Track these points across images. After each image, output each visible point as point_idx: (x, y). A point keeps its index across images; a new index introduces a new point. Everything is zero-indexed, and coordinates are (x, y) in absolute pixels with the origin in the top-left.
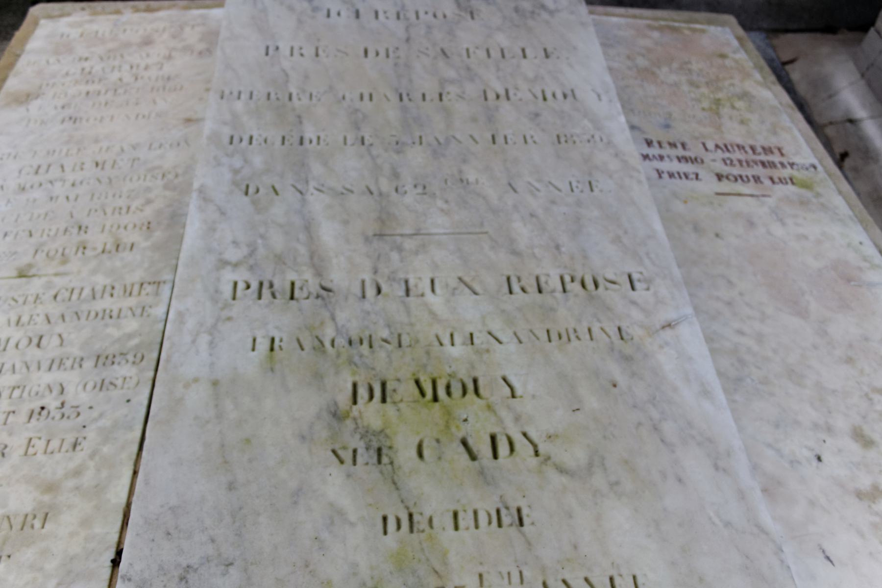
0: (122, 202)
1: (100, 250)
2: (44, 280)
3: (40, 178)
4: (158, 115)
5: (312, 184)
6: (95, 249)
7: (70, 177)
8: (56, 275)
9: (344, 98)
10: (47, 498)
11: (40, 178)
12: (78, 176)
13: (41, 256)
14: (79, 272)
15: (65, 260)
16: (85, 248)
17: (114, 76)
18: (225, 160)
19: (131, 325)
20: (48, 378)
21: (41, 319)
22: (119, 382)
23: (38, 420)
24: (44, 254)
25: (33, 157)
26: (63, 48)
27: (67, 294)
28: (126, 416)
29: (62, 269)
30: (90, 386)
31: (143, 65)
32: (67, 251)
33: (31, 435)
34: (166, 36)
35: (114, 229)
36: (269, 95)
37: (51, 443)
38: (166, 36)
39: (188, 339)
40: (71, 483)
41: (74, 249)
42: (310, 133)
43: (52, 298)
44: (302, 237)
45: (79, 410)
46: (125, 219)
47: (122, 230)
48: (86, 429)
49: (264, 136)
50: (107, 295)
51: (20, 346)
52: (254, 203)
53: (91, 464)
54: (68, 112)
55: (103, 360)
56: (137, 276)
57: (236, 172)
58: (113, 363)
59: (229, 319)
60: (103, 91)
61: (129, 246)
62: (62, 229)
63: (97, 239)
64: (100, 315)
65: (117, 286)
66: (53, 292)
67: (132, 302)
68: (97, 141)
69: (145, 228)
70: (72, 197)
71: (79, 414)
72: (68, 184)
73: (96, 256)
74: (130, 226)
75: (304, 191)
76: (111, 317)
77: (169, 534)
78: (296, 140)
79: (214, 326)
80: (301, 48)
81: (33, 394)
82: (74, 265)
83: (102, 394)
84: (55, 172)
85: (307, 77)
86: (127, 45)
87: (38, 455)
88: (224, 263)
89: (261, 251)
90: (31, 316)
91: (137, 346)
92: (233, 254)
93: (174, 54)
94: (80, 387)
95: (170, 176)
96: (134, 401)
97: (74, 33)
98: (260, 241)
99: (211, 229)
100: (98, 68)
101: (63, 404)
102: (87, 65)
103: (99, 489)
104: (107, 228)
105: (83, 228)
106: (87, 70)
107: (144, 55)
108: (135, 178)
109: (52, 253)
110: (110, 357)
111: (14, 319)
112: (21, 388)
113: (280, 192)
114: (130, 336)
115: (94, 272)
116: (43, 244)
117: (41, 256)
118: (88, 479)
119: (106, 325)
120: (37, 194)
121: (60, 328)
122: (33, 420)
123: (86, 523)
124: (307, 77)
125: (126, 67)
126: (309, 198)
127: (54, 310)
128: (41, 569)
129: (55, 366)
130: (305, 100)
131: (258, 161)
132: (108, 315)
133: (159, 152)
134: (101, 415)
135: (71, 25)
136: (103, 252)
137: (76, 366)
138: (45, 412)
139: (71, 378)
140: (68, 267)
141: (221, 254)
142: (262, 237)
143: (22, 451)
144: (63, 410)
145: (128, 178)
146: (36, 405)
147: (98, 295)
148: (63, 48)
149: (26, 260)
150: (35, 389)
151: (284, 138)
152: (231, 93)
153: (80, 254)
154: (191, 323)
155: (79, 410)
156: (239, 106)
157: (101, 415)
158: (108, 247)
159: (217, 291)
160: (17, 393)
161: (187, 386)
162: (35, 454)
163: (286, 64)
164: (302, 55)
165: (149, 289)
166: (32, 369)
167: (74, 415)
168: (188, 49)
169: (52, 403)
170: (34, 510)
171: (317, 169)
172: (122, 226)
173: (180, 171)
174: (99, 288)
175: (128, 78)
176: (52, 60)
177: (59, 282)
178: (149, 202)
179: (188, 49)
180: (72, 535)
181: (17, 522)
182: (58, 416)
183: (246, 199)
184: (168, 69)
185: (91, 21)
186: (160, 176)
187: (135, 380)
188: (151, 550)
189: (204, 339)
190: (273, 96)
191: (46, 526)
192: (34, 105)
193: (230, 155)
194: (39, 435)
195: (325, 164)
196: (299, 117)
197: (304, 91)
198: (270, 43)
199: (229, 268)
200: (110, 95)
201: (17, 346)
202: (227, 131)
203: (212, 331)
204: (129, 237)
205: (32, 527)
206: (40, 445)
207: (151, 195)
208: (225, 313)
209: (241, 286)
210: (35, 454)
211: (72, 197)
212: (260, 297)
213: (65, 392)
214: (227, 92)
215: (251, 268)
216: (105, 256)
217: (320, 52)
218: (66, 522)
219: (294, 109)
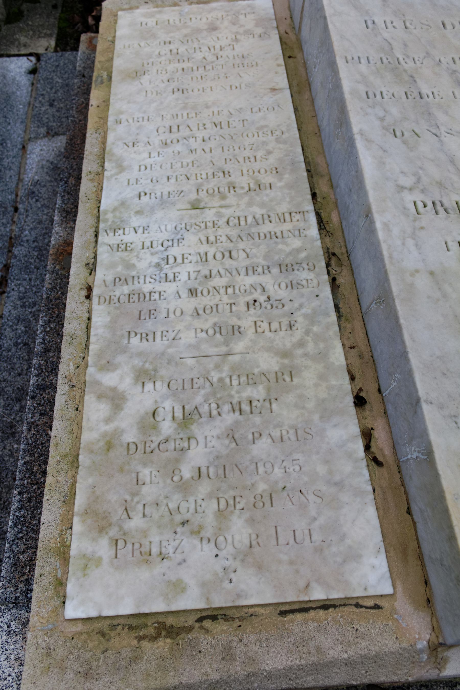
0: (247, 153)
1: (247, 189)
2: (213, 211)
3: (174, 136)
4: (247, 86)
5: (443, 129)
6: (243, 188)
7: (200, 135)
8: (221, 207)
9: (440, 61)
10: (286, 361)
11: (174, 136)
12: (205, 134)
13: (203, 194)
14: (238, 205)
15: (223, 197)
16: (234, 188)
17: (199, 56)
18: (369, 110)
19: (296, 243)
20: (250, 280)
21: (224, 239)
22: (304, 283)
23: (255, 309)
24: (205, 191)
25: (163, 119)
26: (147, 34)
27: (236, 221)
28: (320, 306)
29: (223, 203)
30: (283, 286)
31: (218, 47)
32: (221, 189)
33: (255, 319)
34: (226, 23)
35: (251, 173)
36: (381, 59)
37: (271, 324)
38: (226, 23)
39: (399, 243)
40: (299, 352)
41: (227, 189)
42: (425, 90)
43: (226, 224)
44: (451, 168)
45: (282, 302)
46: (257, 166)
47: (256, 174)
48: (294, 314)
49: (391, 92)
50: (267, 221)
51: (217, 257)
52: (405, 142)
53: (309, 339)
54: (174, 85)
55: (285, 267)
56: (284, 207)
57: (382, 119)
58: (293, 270)
59: (422, 228)
60: (195, 68)
61: (268, 185)
62: (210, 174)
63: (243, 182)
64: (268, 236)
65: (272, 215)
66: (225, 220)
67: (287, 226)
68: (207, 107)
69: (274, 172)
70: (207, 150)
71: (283, 306)
72: (199, 140)
73: (246, 193)
74: (262, 171)
75: (438, 134)
76: (277, 237)
77: (444, 374)
78: (416, 94)
79: (414, 233)
80: (392, 23)
81: (243, 291)
82: (231, 199)
83: (295, 291)
84: (184, 132)
85: (405, 45)
86: (198, 31)
87: (266, 332)
88: (401, 188)
89: (425, 179)
90: (216, 237)
91: (307, 257)
92: (407, 182)
93: (238, 37)
94: (276, 287)
95: (278, 133)
96: (321, 295)
97: (151, 22)
98: (421, 172)
99: (381, 164)
100: (182, 49)
101: (269, 298)
102: (172, 47)
103: (322, 356)
104: (245, 172)
105: (226, 172)
106: (175, 51)
107: (215, 39)
108: (250, 135)
109: (211, 191)
110: (289, 266)
111: (204, 239)
112: (232, 287)
113: (420, 135)
114: (298, 251)
115: (250, 204)
116: (201, 185)
117: (203, 194)
118: (310, 347)
119: (276, 243)
120: (178, 147)
121: (241, 245)
122: (251, 309)
123: (322, 377)
124: (405, 45)
125: (205, 49)
126: (442, 138)
127: (234, 233)
128: (304, 408)
129: (250, 272)
130: (411, 64)
131: (394, 111)
132: (272, 236)
133: (261, 114)
134: (301, 306)
135: (145, 15)
136: (250, 190)
137: (266, 271)
138: (257, 304)
139: (267, 280)
140: (227, 202)
141: (396, 181)
142: (421, 168)
143: (253, 330)
144: (271, 302)
145: (245, 135)
146: (250, 298)
147: (261, 222)
148: (147, 34)
149: (193, 196)
150: (243, 288)
151: (406, 93)
152: (353, 59)
153: (232, 191)
154: (396, 231)
155: (282, 302)
156: (363, 67)
157: (301, 306)
158: (252, 186)
159: (405, 208)
160: (230, 291)
161: (412, 275)
162: (263, 332)
163: (386, 35)
164: (394, 27)
165: (298, 217)
166: (233, 274)
167: (280, 306)
168: (248, 33)
169: (262, 299)
170: (280, 369)
171: (441, 117)
172: (256, 171)
173: (284, 129)
174: (258, 216)
175: (211, 58)
176: (142, 44)
177: (227, 212)
178: (269, 153)
179: (248, 33)
180: (316, 385)
181: (272, 377)
182: (269, 307)
183: (398, 141)
184: (239, 49)
185: (160, 12)
186: (269, 133)
187: (315, 281)
188: (437, 384)
189: (410, 242)
190: (384, 60)
191: (294, 379)
192: (145, 79)
193: (373, 107)
194: (261, 319)
195: (446, 113)
196: (412, 77)
197: (408, 57)
198: (367, 18)
199: (406, 191)
200: (201, 70)
201: (214, 257)
202: (362, 88)
203: (413, 236)
204: (267, 179)
205: (284, 380)
206: (265, 326)
207: (270, 147)
208: (417, 224)
209: (420, 205)
210: (263, 332)
211: (207, 150)
212: (437, 213)
213: (266, 290)
214: (349, 58)
215: (423, 191)
216: (253, 193)
217: (408, 24)
218: (309, 376)
219: (405, 71)
